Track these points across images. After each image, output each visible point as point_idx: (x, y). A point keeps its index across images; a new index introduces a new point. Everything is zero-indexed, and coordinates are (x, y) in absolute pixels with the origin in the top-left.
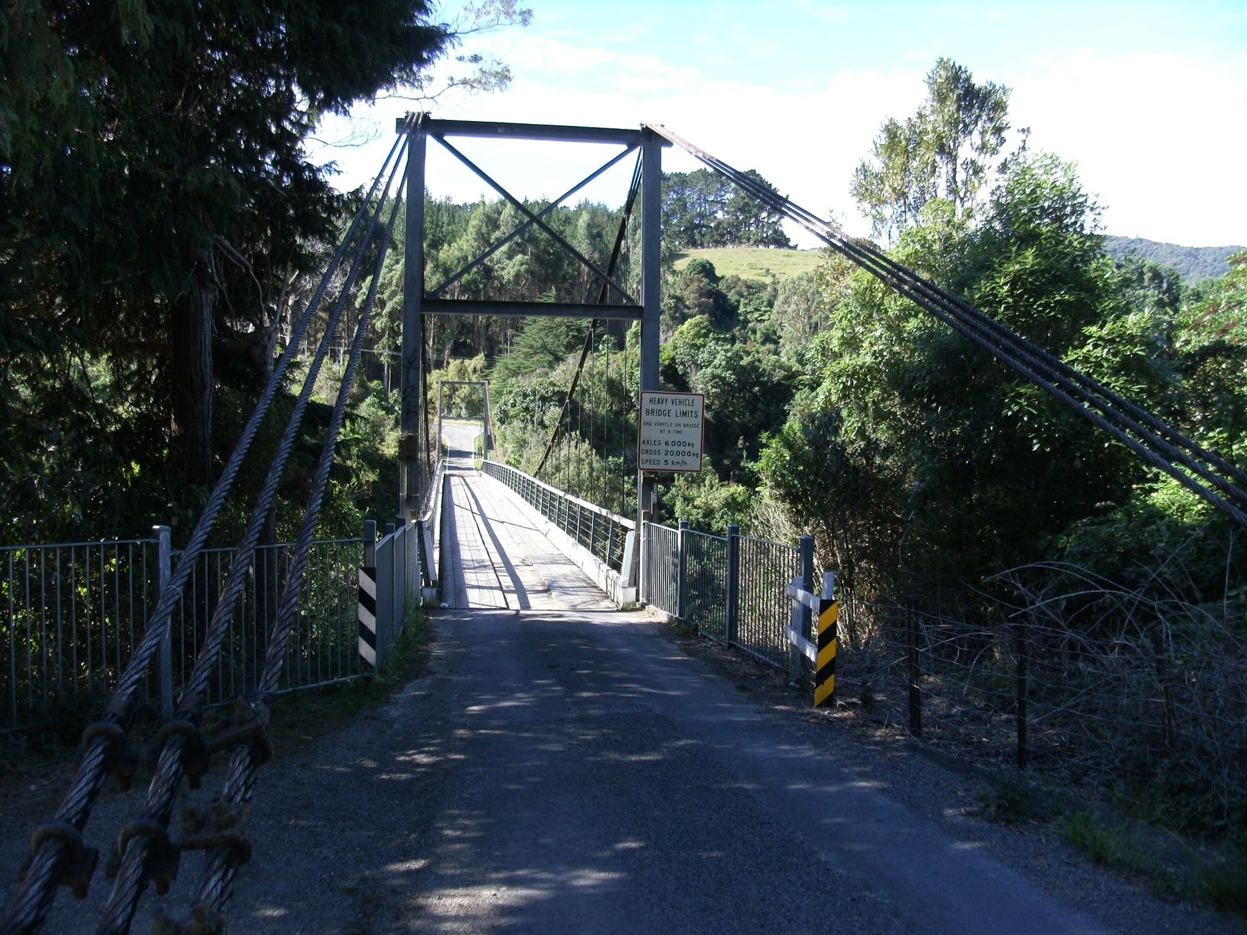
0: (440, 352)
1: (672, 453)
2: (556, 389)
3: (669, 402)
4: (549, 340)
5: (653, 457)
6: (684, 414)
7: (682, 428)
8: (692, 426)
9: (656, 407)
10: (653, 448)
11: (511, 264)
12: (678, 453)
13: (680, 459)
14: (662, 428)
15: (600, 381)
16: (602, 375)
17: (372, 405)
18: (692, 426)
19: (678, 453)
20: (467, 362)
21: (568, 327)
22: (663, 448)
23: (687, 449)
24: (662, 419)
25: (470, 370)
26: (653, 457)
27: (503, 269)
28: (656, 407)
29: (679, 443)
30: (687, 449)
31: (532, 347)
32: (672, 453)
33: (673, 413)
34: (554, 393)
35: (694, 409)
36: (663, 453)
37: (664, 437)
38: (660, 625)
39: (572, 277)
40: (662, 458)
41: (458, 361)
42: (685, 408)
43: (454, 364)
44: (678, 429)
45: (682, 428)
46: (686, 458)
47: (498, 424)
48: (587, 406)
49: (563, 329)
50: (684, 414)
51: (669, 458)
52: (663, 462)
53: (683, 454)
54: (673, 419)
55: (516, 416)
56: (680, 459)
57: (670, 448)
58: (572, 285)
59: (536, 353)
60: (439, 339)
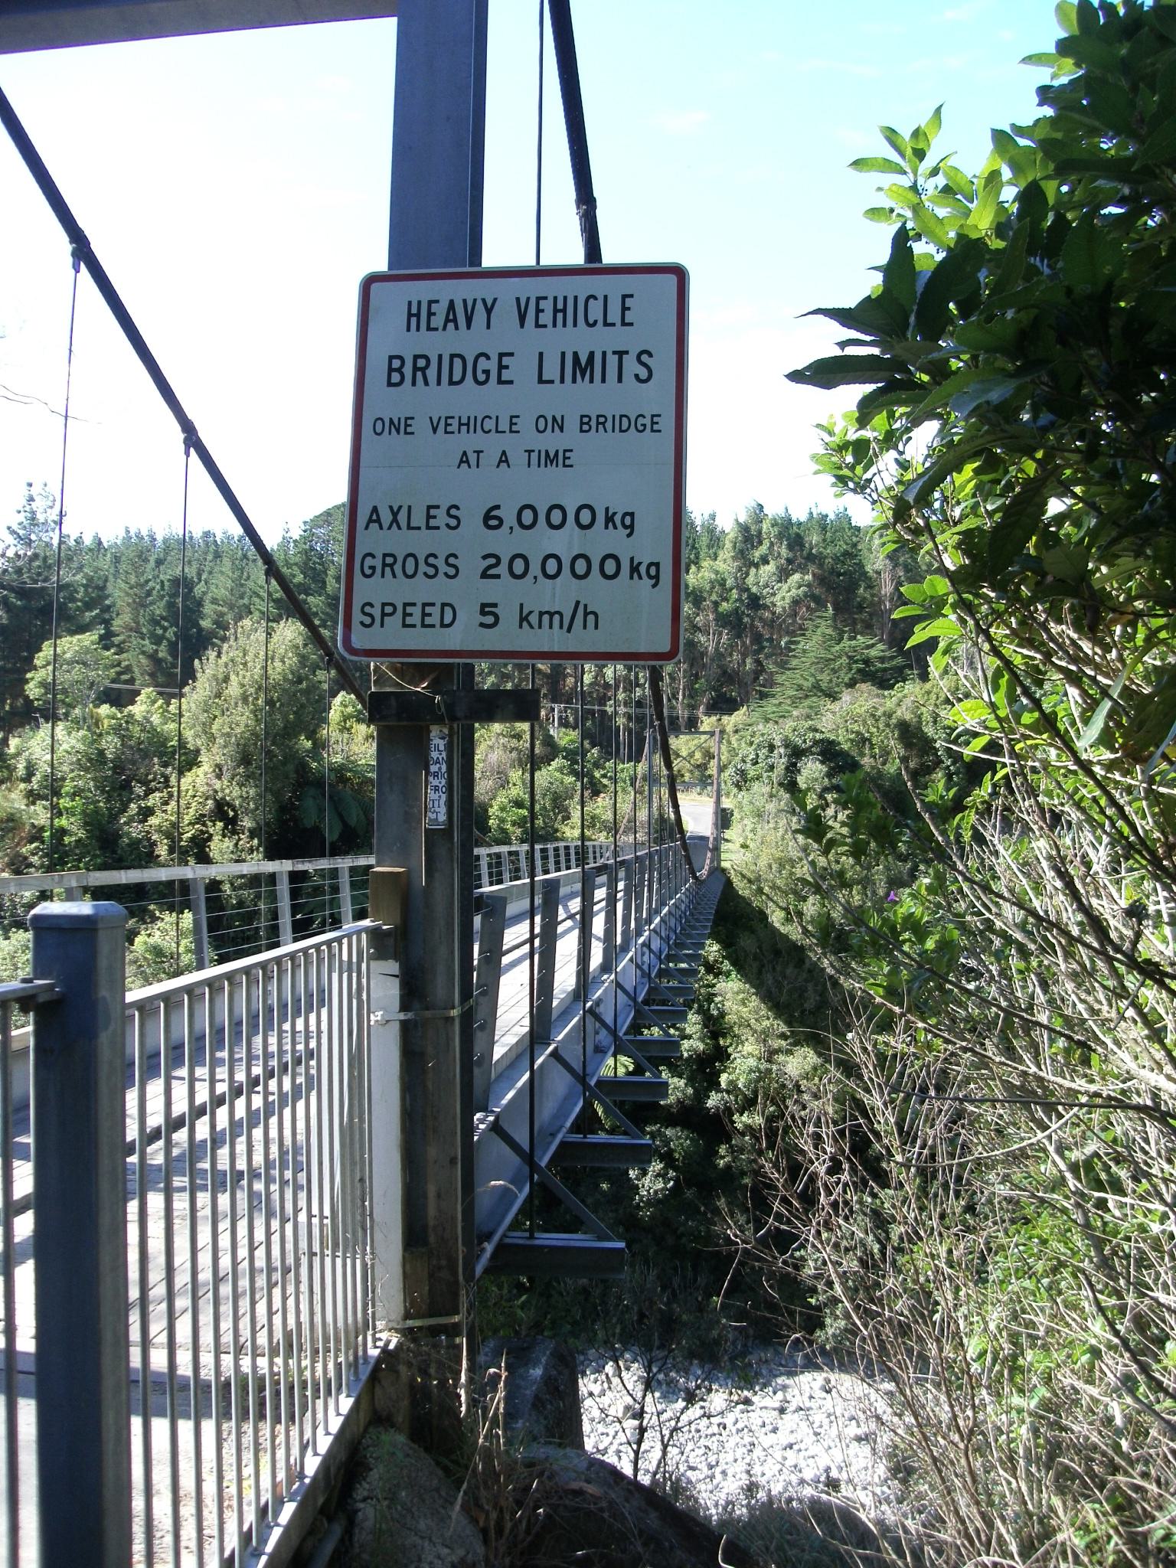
0: (693, 707)
1: (519, 567)
2: (818, 736)
3: (506, 313)
4: (825, 677)
5: (420, 590)
6: (583, 367)
7: (570, 438)
8: (625, 424)
9: (438, 344)
10: (421, 543)
11: (785, 587)
12: (552, 567)
13: (561, 594)
14: (469, 441)
15: (888, 725)
16: (890, 716)
17: (560, 770)
18: (625, 424)
19: (552, 567)
20: (725, 718)
21: (850, 658)
22: (472, 542)
23: (602, 541)
24: (467, 400)
25: (729, 729)
26: (420, 590)
27: (774, 594)
28: (438, 344)
29: (556, 517)
30: (602, 541)
31: (800, 688)
32: (519, 567)
33: (521, 369)
34: (816, 742)
35: (630, 340)
36: (471, 564)
37: (474, 491)
38: (355, 1408)
39: (872, 604)
40: (467, 592)
41: (714, 718)
42: (582, 340)
43: (707, 723)
44: (552, 442)
45: (570, 438)
46: (596, 591)
47: (735, 790)
48: (866, 761)
49: (844, 660)
50: (583, 367)
51: (505, 592)
52: (468, 616)
53: (581, 567)
54: (524, 397)
55: (758, 778)
56: (561, 594)
57: (504, 543)
58: (871, 615)
59: (807, 696)
60: (692, 694)
